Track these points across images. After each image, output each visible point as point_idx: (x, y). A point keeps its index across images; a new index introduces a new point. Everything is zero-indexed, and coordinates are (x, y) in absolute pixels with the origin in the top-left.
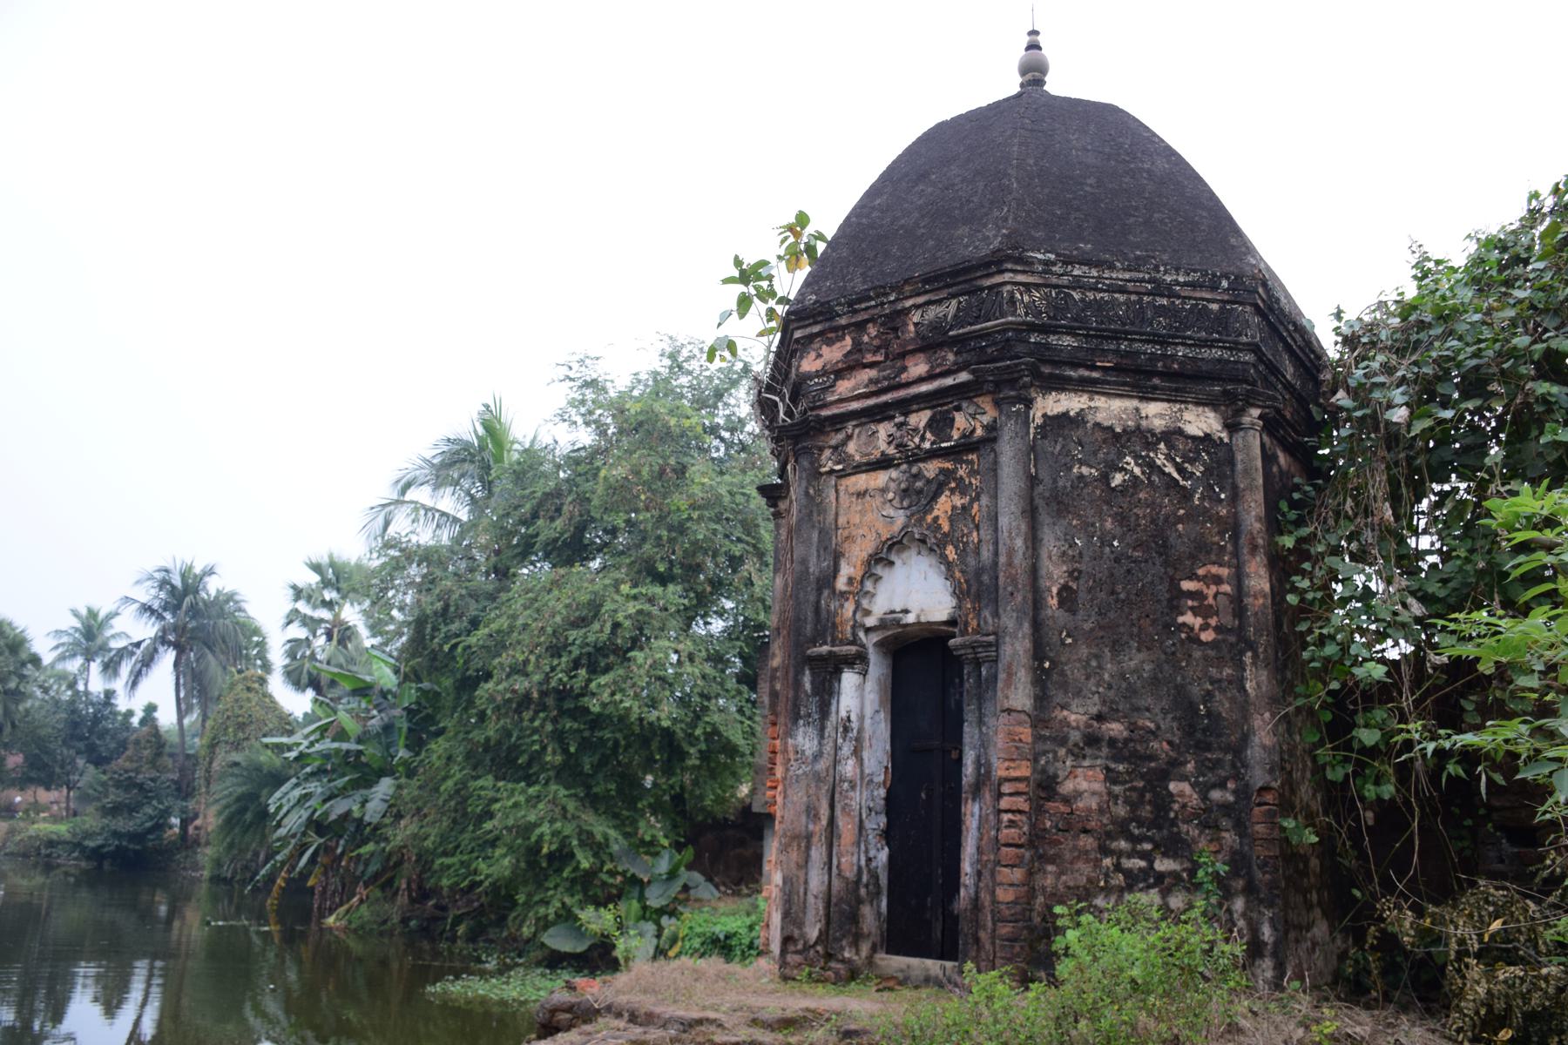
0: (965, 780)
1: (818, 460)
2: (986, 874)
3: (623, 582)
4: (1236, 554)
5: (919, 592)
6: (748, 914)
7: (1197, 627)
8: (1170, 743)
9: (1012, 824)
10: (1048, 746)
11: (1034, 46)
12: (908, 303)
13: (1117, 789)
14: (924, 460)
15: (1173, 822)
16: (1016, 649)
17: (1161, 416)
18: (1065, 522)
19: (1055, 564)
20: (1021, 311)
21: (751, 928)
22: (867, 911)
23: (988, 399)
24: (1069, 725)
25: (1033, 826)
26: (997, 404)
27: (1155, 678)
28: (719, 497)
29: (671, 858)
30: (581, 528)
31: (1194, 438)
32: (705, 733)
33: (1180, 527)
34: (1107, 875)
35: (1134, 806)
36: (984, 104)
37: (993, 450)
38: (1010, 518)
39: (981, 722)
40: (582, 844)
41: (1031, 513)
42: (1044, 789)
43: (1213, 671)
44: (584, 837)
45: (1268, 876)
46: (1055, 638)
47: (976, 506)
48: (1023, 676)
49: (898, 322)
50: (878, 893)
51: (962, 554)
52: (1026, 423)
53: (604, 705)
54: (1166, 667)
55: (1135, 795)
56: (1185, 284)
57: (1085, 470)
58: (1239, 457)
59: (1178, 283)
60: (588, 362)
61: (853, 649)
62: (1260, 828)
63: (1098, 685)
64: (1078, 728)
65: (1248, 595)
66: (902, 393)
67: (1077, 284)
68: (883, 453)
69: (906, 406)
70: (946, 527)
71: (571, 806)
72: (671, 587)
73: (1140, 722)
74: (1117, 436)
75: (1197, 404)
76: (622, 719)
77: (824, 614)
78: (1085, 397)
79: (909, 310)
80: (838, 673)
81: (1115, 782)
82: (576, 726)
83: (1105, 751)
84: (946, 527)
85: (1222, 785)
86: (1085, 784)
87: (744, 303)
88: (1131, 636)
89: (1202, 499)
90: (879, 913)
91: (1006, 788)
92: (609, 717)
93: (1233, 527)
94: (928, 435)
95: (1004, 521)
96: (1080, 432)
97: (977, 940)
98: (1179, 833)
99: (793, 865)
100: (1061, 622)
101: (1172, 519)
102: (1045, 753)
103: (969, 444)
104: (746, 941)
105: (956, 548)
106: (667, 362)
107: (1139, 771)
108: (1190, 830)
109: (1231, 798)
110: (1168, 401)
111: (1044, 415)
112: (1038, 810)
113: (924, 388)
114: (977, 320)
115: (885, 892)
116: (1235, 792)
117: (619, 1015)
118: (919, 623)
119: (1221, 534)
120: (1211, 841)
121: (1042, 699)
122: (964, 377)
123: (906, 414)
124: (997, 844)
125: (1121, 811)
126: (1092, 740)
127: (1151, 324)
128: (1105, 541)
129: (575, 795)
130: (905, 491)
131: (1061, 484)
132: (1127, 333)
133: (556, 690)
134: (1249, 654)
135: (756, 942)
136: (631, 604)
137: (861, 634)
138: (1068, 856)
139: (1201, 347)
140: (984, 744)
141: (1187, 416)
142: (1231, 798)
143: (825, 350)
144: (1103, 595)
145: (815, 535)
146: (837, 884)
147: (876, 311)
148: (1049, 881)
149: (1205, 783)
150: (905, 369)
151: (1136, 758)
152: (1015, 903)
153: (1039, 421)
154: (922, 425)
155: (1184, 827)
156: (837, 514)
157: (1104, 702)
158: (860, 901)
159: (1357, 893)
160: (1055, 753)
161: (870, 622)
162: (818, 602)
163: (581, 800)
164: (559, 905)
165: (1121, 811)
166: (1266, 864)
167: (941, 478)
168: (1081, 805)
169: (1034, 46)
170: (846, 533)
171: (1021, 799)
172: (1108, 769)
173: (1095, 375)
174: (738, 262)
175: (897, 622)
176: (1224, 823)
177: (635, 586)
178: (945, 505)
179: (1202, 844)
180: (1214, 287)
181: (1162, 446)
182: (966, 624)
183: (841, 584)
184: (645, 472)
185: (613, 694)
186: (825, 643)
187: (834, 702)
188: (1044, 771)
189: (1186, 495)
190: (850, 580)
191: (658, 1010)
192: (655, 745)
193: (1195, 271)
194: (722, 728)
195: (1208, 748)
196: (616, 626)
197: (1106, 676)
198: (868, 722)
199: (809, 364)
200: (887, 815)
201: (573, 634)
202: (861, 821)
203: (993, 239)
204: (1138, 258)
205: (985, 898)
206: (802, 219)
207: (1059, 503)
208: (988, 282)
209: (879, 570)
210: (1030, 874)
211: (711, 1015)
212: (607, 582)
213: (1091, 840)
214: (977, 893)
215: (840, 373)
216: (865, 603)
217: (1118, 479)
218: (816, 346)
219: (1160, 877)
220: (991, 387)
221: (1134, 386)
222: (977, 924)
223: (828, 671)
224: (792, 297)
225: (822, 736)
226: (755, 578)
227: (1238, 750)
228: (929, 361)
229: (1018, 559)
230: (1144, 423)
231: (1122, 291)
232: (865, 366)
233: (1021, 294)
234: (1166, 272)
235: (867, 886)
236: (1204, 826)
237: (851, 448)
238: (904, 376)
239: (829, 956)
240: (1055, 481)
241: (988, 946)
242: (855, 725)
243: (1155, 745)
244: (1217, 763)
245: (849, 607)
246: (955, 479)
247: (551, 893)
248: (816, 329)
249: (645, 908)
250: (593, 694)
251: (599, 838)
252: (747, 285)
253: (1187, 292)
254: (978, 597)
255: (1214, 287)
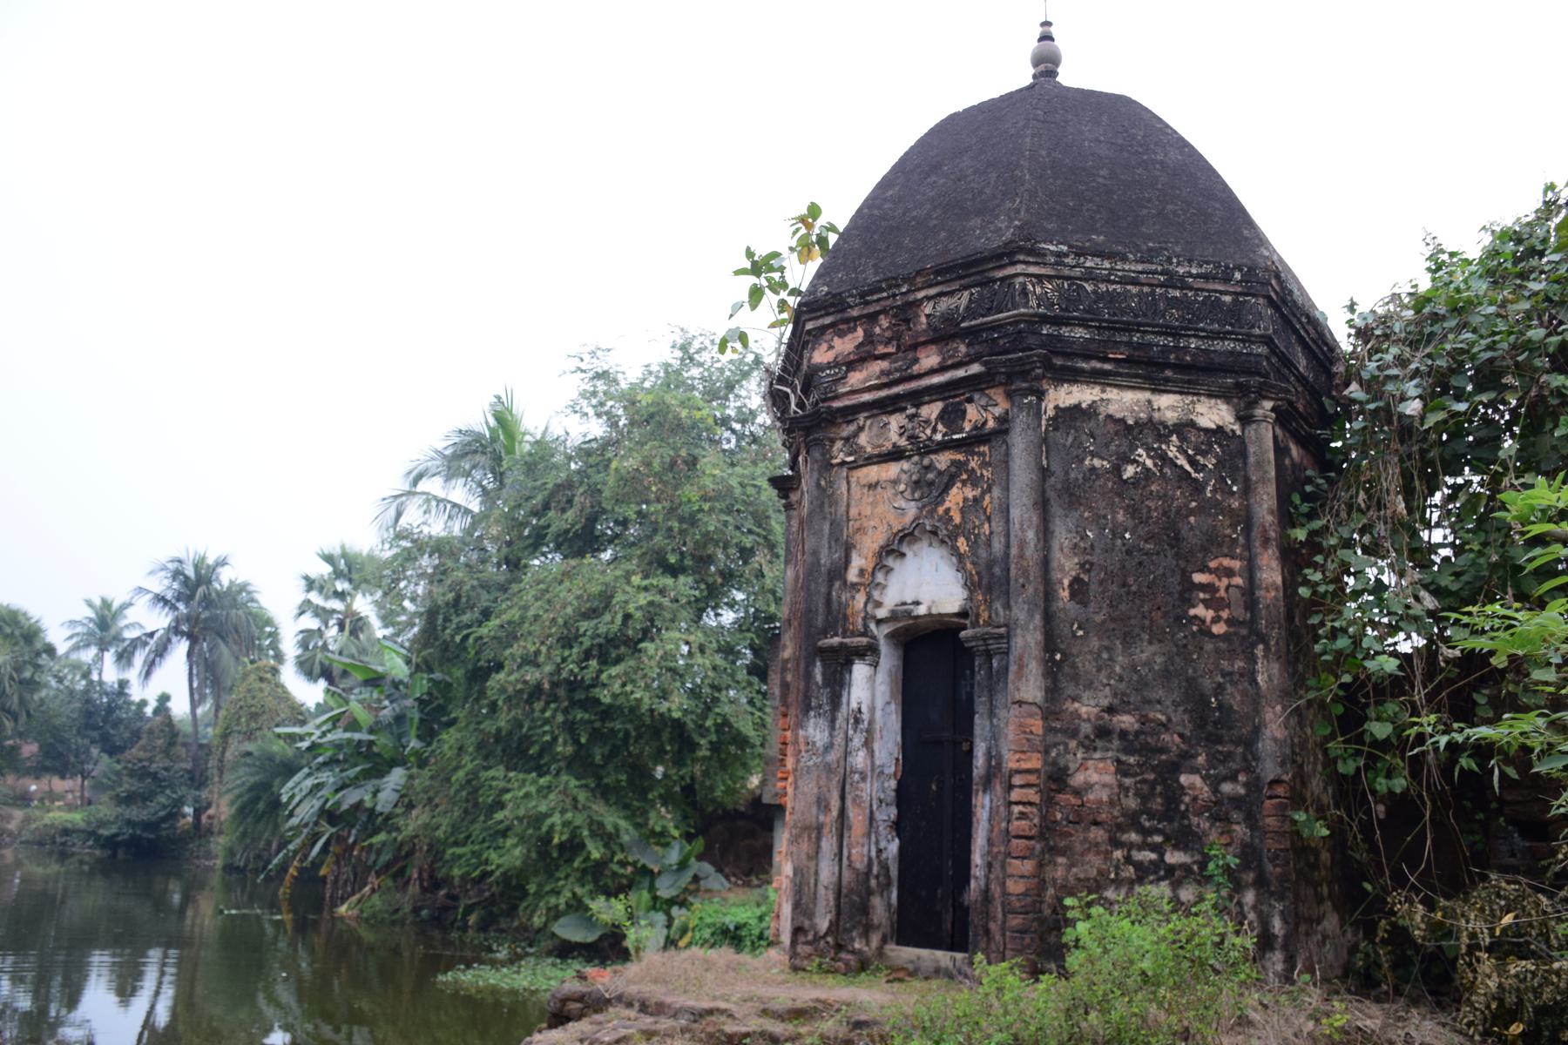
0: (975, 772)
1: (830, 451)
2: (997, 865)
3: (634, 573)
4: (1248, 546)
5: (930, 584)
6: (758, 905)
7: (1208, 619)
8: (1181, 736)
9: (1023, 816)
10: (1059, 737)
11: (1046, 37)
12: (920, 295)
13: (1128, 781)
14: (935, 452)
15: (1184, 815)
16: (1028, 641)
17: (1173, 408)
18: (1077, 515)
19: (1066, 556)
20: (1033, 303)
21: (761, 919)
22: (877, 901)
23: (1000, 390)
24: (1079, 717)
25: (1043, 818)
26: (1009, 396)
27: (1167, 670)
28: (730, 489)
29: (682, 849)
30: (592, 520)
31: (1207, 431)
32: (716, 724)
33: (1192, 519)
34: (1117, 867)
35: (1144, 799)
36: (996, 95)
37: (1005, 442)
38: (1021, 511)
39: (992, 714)
40: (593, 835)
41: (1043, 505)
42: (1055, 781)
43: (1224, 664)
44: (595, 827)
45: (1278, 870)
46: (1066, 631)
47: (987, 498)
48: (1034, 668)
49: (910, 314)
50: (889, 884)
51: (974, 546)
52: (1038, 415)
53: (615, 696)
54: (1178, 659)
55: (1145, 788)
56: (1198, 276)
57: (1097, 462)
58: (1252, 449)
59: (1191, 275)
60: (599, 353)
61: (864, 640)
62: (1270, 821)
63: (1109, 678)
64: (1089, 720)
65: (1260, 588)
66: (914, 385)
67: (1090, 275)
68: (894, 445)
69: (917, 398)
70: (957, 519)
71: (582, 796)
72: (682, 579)
73: (1151, 715)
74: (1129, 428)
75: (1210, 396)
76: (632, 710)
77: (835, 606)
78: (1097, 389)
79: (921, 301)
80: (848, 664)
81: (1125, 774)
82: (587, 716)
83: (1116, 743)
84: (957, 519)
85: (1233, 778)
86: (1096, 776)
87: (756, 295)
88: (1143, 628)
89: (1214, 491)
90: (889, 905)
91: (1017, 780)
92: (620, 708)
93: (1245, 519)
94: (940, 427)
95: (1015, 513)
96: (1092, 424)
97: (987, 932)
98: (1190, 825)
99: (804, 857)
100: (1072, 614)
101: (1184, 512)
102: (1055, 745)
103: (980, 437)
104: (756, 932)
105: (968, 539)
106: (679, 354)
107: (1151, 767)
108: (1201, 823)
109: (1242, 791)
110: (1181, 393)
111: (1056, 407)
112: (1048, 802)
113: (936, 380)
114: (989, 311)
115: (895, 884)
116: (1246, 785)
117: (630, 1005)
118: (930, 615)
119: (1233, 526)
120: (1222, 833)
121: (1053, 692)
122: (976, 368)
123: (918, 406)
124: (1008, 835)
125: (1132, 803)
126: (1103, 732)
127: (1163, 316)
128: (1117, 533)
129: (586, 786)
130: (917, 483)
131: (1072, 475)
132: (1139, 325)
133: (567, 681)
134: (1261, 647)
135: (766, 933)
136: (643, 595)
137: (872, 626)
138: (1078, 848)
139: (1213, 339)
140: (995, 736)
141: (1199, 408)
142: (1242, 791)
143: (837, 342)
144: (1114, 587)
145: (826, 527)
146: (847, 875)
147: (888, 303)
148: (1060, 873)
149: (1216, 776)
150: (916, 360)
151: (1147, 750)
152: (1025, 894)
153: (1051, 413)
154: (934, 416)
155: (1195, 820)
156: (848, 506)
157: (1115, 695)
158: (870, 892)
159: (1368, 887)
160: (1066, 745)
161: (882, 613)
162: (829, 594)
163: (593, 790)
164: (569, 895)
165: (1132, 803)
166: (1276, 857)
167: (953, 469)
168: (1091, 797)
169: (1046, 37)
170: (857, 525)
171: (1032, 791)
172: (1118, 761)
173: (1107, 367)
174: (749, 254)
175: (908, 614)
176: (1235, 816)
177: (646, 577)
178: (956, 497)
179: (1213, 836)
180: (1227, 279)
181: (1174, 438)
182: (978, 616)
183: (852, 576)
184: (656, 463)
185: (624, 685)
186: (836, 634)
187: (845, 694)
188: (1054, 763)
189: (1198, 488)
190: (862, 572)
191: (668, 1000)
192: (665, 736)
193: (1208, 263)
194: (732, 720)
195: (1220, 740)
196: (627, 617)
197: (1118, 669)
198: (878, 714)
199: (821, 356)
200: (898, 806)
201: (584, 625)
202: (872, 812)
203: (1005, 230)
204: (1150, 250)
205: (996, 890)
206: (814, 211)
207: (1071, 495)
208: (1000, 274)
209: (890, 562)
210: (1041, 865)
211: (722, 1005)
212: (618, 573)
213: (1101, 832)
214: (987, 885)
215: (852, 365)
216: (876, 595)
217: (1130, 471)
218: (828, 337)
219: (1171, 870)
220: (1003, 379)
221: (1147, 378)
222: (988, 916)
223: (839, 663)
224: (803, 288)
225: (832, 727)
226: (766, 570)
227: (1250, 742)
228: (941, 353)
229: (1030, 551)
230: (1156, 415)
231: (1135, 282)
232: (877, 358)
233: (1033, 286)
234: (1179, 264)
235: (877, 877)
236: (1215, 818)
237: (863, 439)
238: (915, 368)
239: (839, 947)
240: (1067, 473)
241: (998, 937)
242: (866, 716)
243: (1166, 737)
244: (1229, 756)
245: (860, 599)
246: (966, 471)
247: (561, 883)
248: (828, 320)
249: (655, 898)
250: (604, 685)
251: (610, 828)
252: (758, 276)
253: (1199, 284)
254: (989, 590)
255: (1227, 279)
